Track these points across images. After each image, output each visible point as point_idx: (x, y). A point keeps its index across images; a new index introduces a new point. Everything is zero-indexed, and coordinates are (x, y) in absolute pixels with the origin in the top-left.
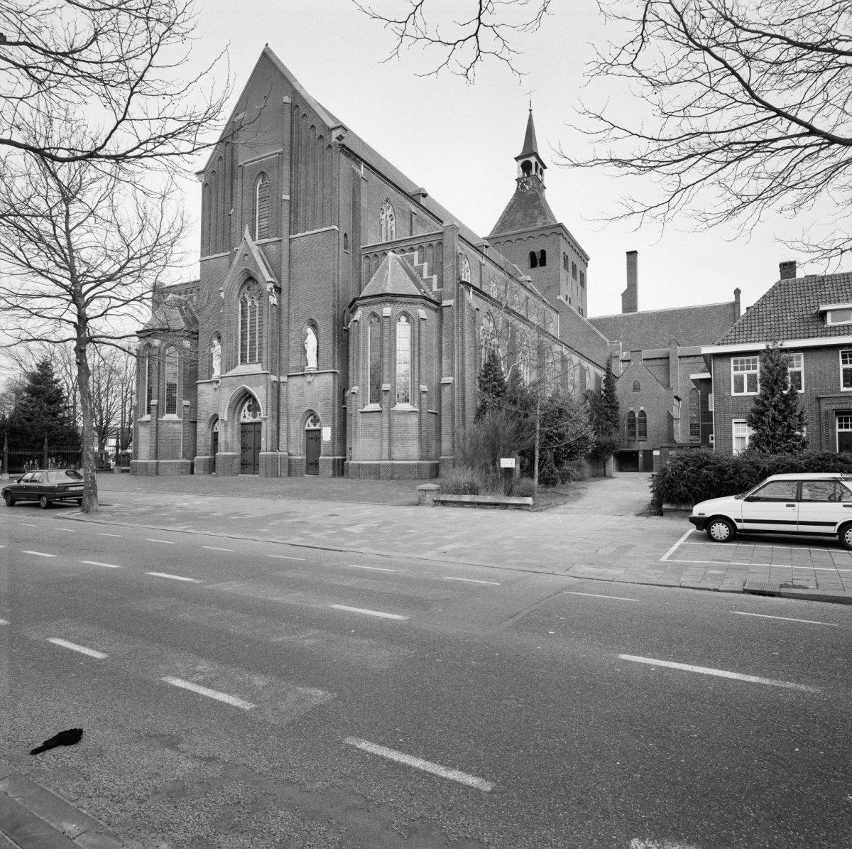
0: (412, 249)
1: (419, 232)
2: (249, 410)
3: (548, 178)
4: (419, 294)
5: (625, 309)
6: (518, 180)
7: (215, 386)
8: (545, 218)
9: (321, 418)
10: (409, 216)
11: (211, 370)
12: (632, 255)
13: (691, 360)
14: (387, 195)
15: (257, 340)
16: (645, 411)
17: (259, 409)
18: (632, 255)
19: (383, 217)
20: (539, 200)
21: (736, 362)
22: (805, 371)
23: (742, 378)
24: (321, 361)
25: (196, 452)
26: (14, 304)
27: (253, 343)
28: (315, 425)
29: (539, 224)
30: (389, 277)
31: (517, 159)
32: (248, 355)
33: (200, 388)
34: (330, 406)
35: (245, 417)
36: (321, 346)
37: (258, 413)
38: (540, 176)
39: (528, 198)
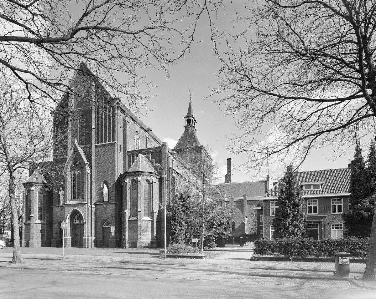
0: (149, 153)
1: (149, 146)
2: (77, 219)
3: (197, 126)
4: (152, 172)
5: (226, 182)
6: (185, 127)
7: (61, 208)
8: (196, 143)
9: (110, 223)
10: (145, 139)
11: (59, 201)
12: (229, 160)
13: (251, 202)
14: (136, 129)
15: (81, 189)
16: (235, 222)
17: (82, 218)
18: (229, 160)
19: (135, 138)
20: (194, 135)
21: (309, 201)
22: (343, 205)
23: (335, 206)
24: (110, 199)
25: (52, 237)
26: (1, 166)
27: (79, 190)
28: (107, 226)
29: (194, 145)
30: (140, 165)
31: (185, 118)
32: (77, 195)
33: (54, 209)
34: (114, 218)
35: (75, 222)
36: (110, 192)
37: (82, 220)
38: (194, 125)
39: (189, 135)
